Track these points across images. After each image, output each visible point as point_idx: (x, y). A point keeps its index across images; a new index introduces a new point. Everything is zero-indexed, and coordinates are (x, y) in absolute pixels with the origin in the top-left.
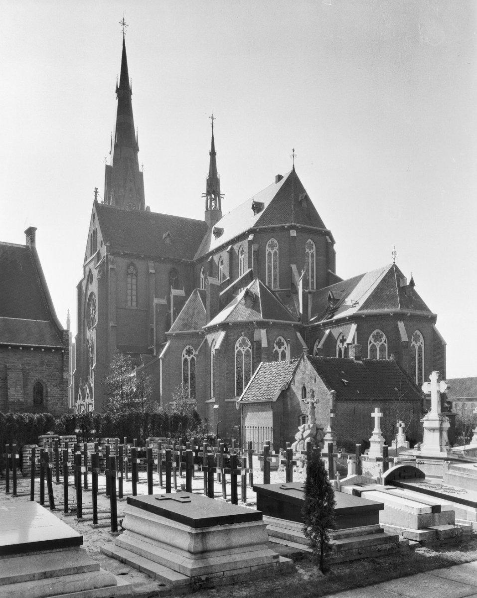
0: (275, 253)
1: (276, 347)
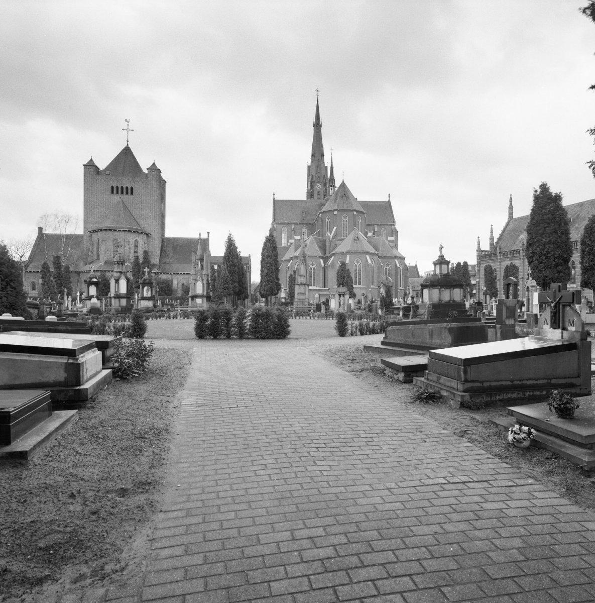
0: (346, 221)
1: (311, 266)
